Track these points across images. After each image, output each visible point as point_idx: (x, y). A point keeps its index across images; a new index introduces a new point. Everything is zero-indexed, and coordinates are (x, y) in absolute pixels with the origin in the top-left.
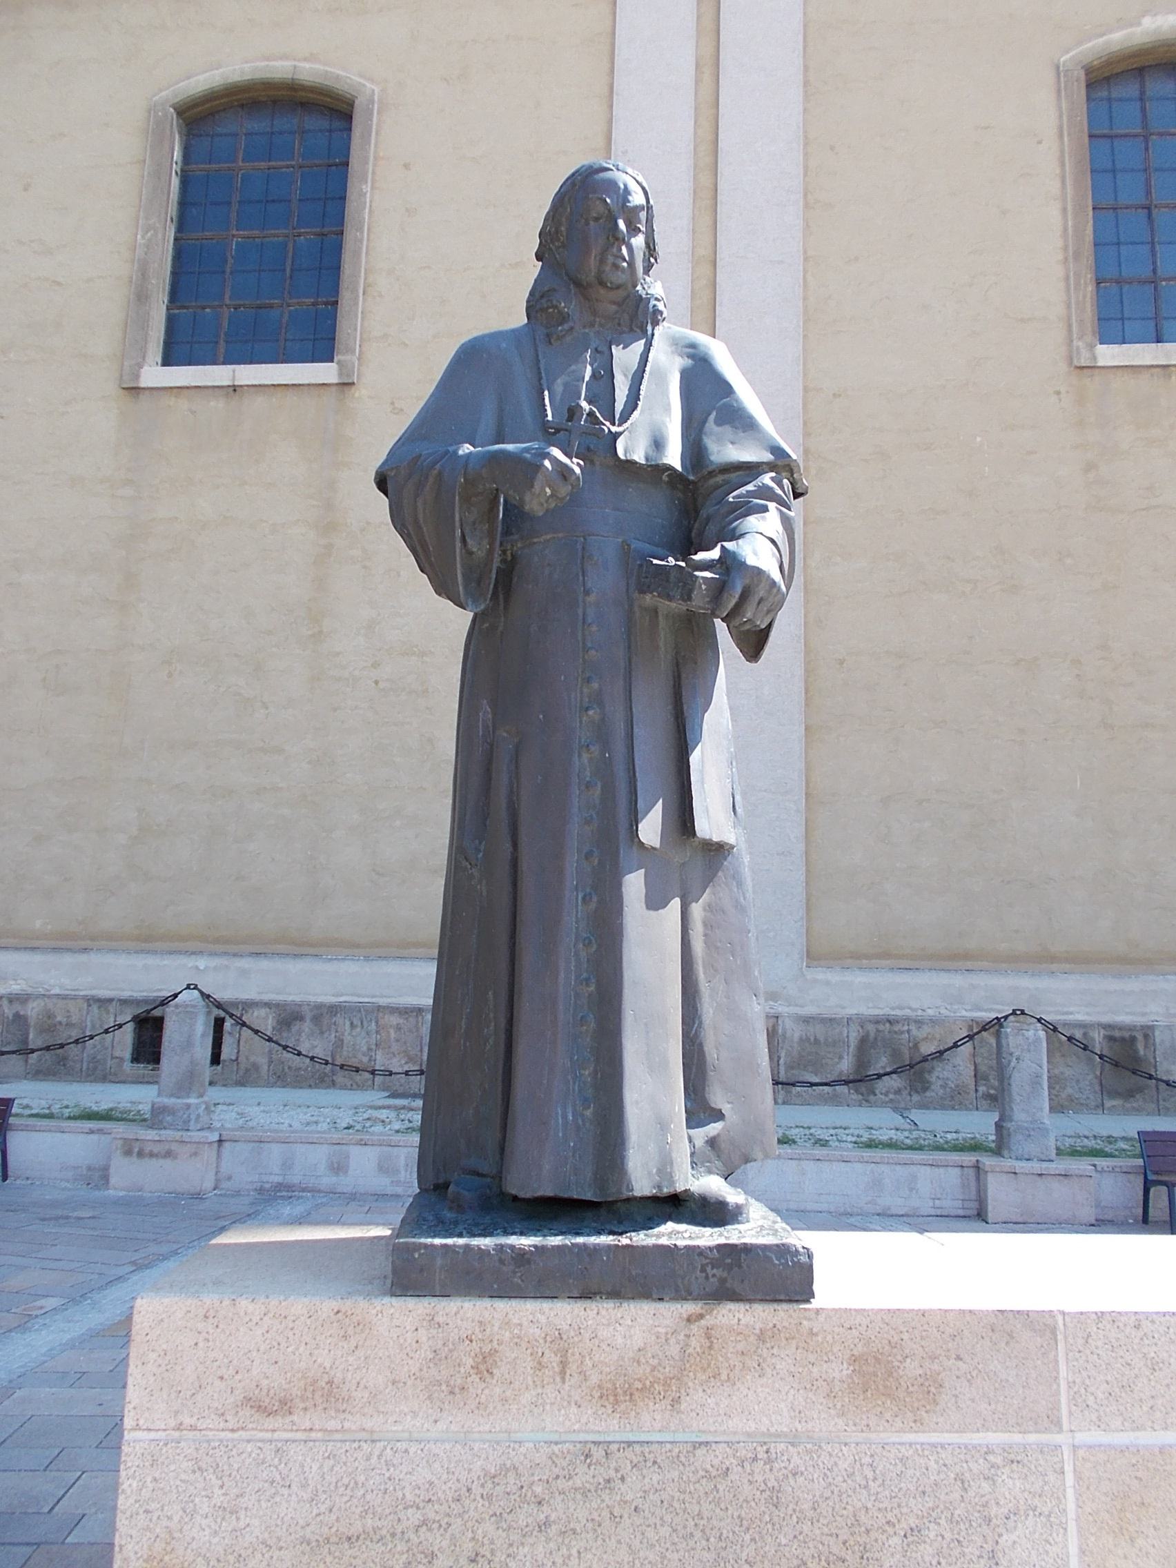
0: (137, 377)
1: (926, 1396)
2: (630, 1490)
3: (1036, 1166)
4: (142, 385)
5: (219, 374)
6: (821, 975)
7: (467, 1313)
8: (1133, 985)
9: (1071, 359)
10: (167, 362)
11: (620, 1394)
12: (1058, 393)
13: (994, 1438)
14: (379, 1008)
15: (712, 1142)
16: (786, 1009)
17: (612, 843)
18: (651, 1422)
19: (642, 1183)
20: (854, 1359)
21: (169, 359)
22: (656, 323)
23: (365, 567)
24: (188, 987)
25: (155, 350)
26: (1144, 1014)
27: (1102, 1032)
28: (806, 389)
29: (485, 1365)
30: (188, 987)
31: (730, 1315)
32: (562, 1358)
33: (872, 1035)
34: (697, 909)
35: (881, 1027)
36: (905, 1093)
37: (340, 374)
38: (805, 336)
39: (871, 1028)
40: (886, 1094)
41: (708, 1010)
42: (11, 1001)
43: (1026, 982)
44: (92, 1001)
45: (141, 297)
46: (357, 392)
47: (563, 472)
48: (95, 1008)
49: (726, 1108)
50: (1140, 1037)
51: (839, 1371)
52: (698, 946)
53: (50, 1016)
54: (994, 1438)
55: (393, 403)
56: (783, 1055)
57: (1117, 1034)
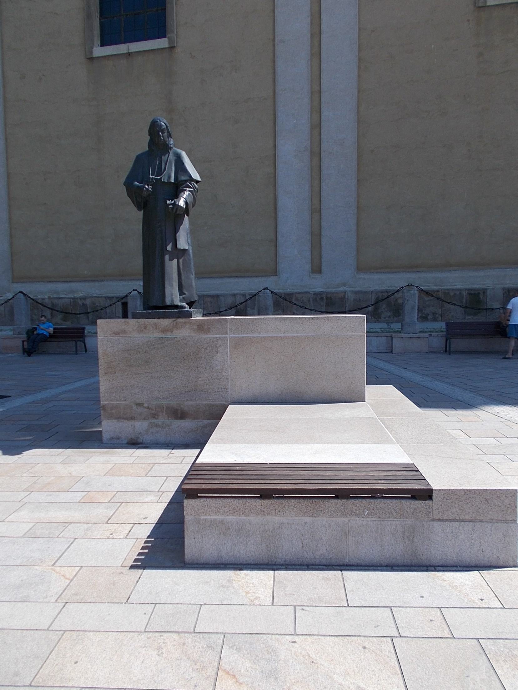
0: (91, 53)
1: (208, 331)
2: (166, 343)
3: (410, 335)
4: (94, 56)
5: (122, 48)
6: (362, 276)
7: (142, 321)
8: (481, 273)
9: (475, 3)
10: (102, 45)
11: (164, 331)
12: (468, 21)
13: (218, 336)
14: (204, 295)
15: (183, 298)
16: (349, 289)
17: (163, 251)
18: (169, 335)
19: (168, 302)
20: (198, 326)
21: (103, 44)
22: (171, 150)
23: (186, 127)
24: (134, 290)
25: (97, 41)
26: (484, 284)
27: (467, 292)
28: (360, 29)
29: (145, 328)
30: (134, 290)
31: (180, 320)
32: (156, 326)
33: (380, 297)
34: (181, 261)
35: (384, 294)
36: (392, 317)
37: (169, 43)
38: (359, 4)
39: (380, 295)
40: (385, 318)
41: (183, 277)
42: (80, 299)
43: (439, 275)
44: (107, 298)
45: (89, 16)
46: (178, 50)
47: (147, 189)
48: (108, 301)
49: (186, 293)
50: (481, 293)
51: (195, 327)
52: (181, 266)
53: (94, 304)
54: (218, 336)
55: (191, 54)
56: (347, 305)
57: (472, 292)
